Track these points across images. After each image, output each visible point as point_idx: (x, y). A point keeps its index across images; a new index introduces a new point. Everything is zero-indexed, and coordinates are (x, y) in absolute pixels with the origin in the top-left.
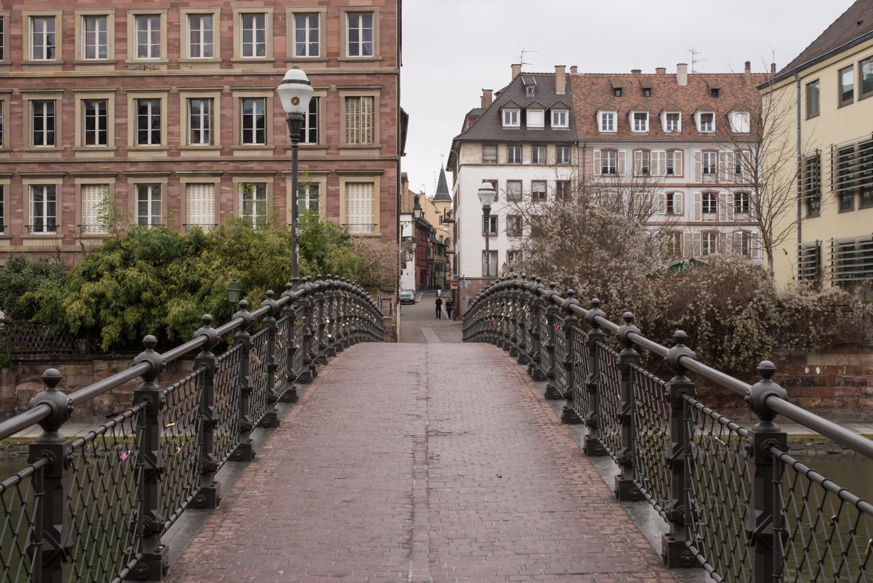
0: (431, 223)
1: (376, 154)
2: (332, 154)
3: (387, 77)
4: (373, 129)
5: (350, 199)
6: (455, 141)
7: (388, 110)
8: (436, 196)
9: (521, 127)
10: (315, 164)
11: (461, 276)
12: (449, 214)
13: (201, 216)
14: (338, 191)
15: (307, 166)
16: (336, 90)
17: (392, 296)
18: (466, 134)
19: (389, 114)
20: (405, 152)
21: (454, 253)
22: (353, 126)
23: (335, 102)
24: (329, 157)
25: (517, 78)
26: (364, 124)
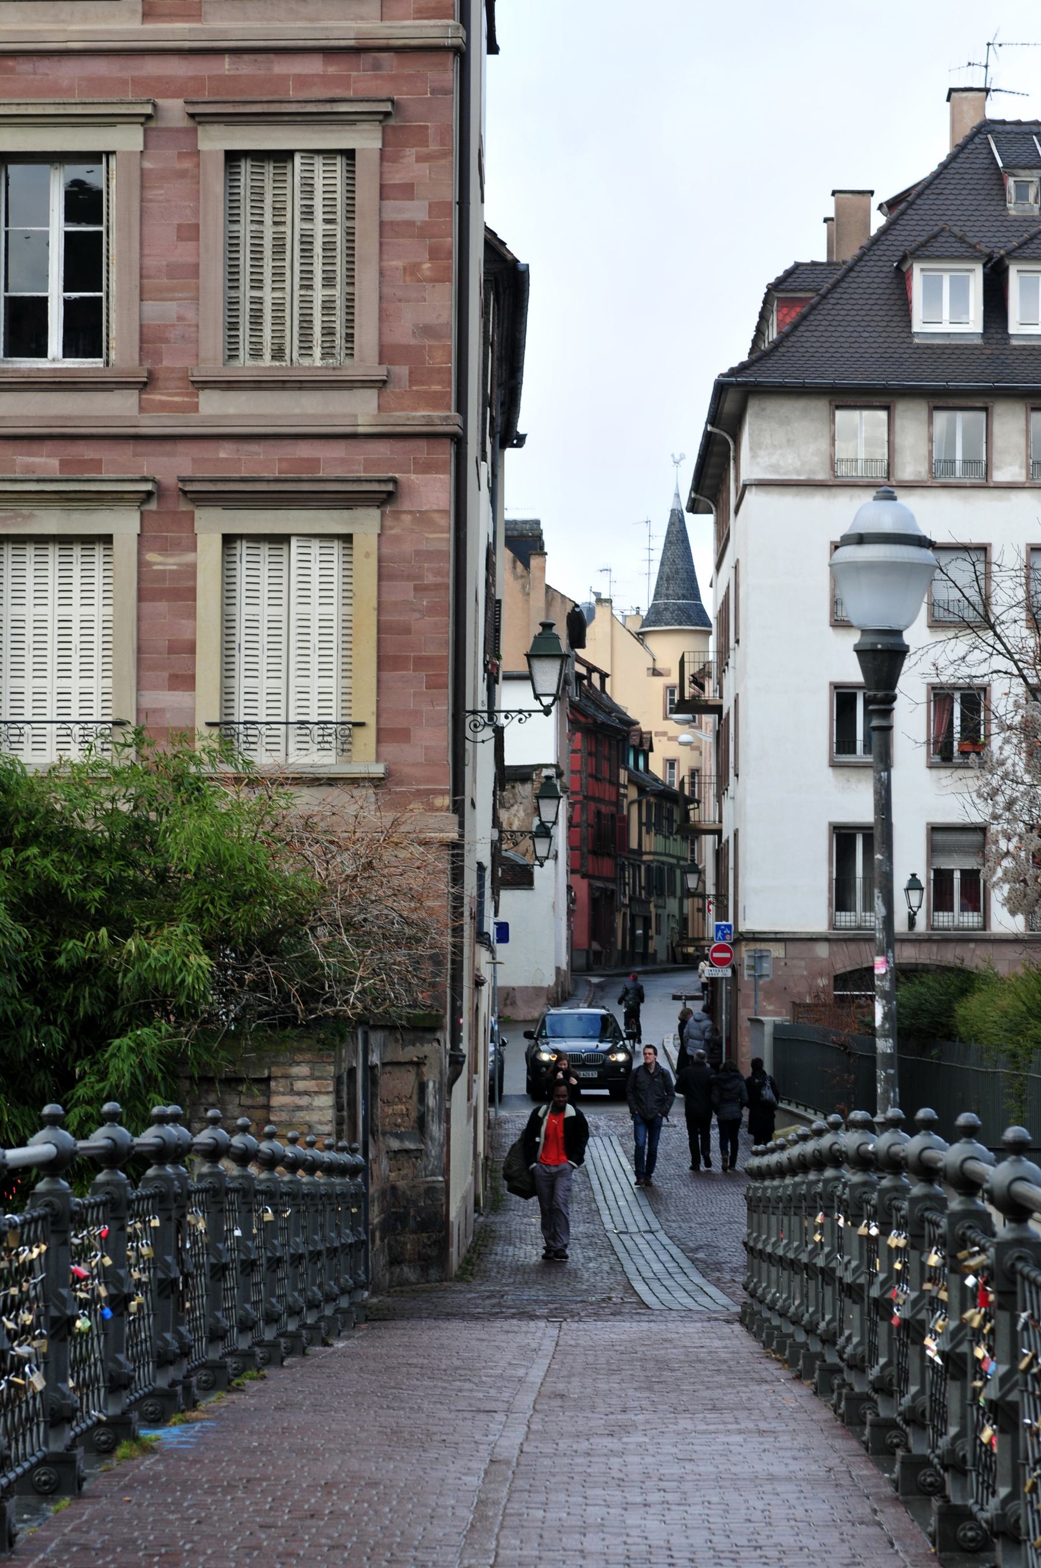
0: (632, 714)
2: (164, 406)
3: (412, 66)
4: (350, 299)
5: (243, 611)
6: (721, 388)
7: (416, 211)
8: (654, 610)
9: (985, 334)
10: (87, 452)
11: (746, 925)
12: (698, 682)
13: (51, 684)
14: (191, 572)
15: (55, 462)
16: (186, 123)
17: (427, 1049)
18: (770, 363)
19: (421, 231)
20: (521, 428)
21: (718, 832)
22: (257, 284)
23: (182, 174)
24: (151, 424)
25: (970, 139)
26: (307, 276)
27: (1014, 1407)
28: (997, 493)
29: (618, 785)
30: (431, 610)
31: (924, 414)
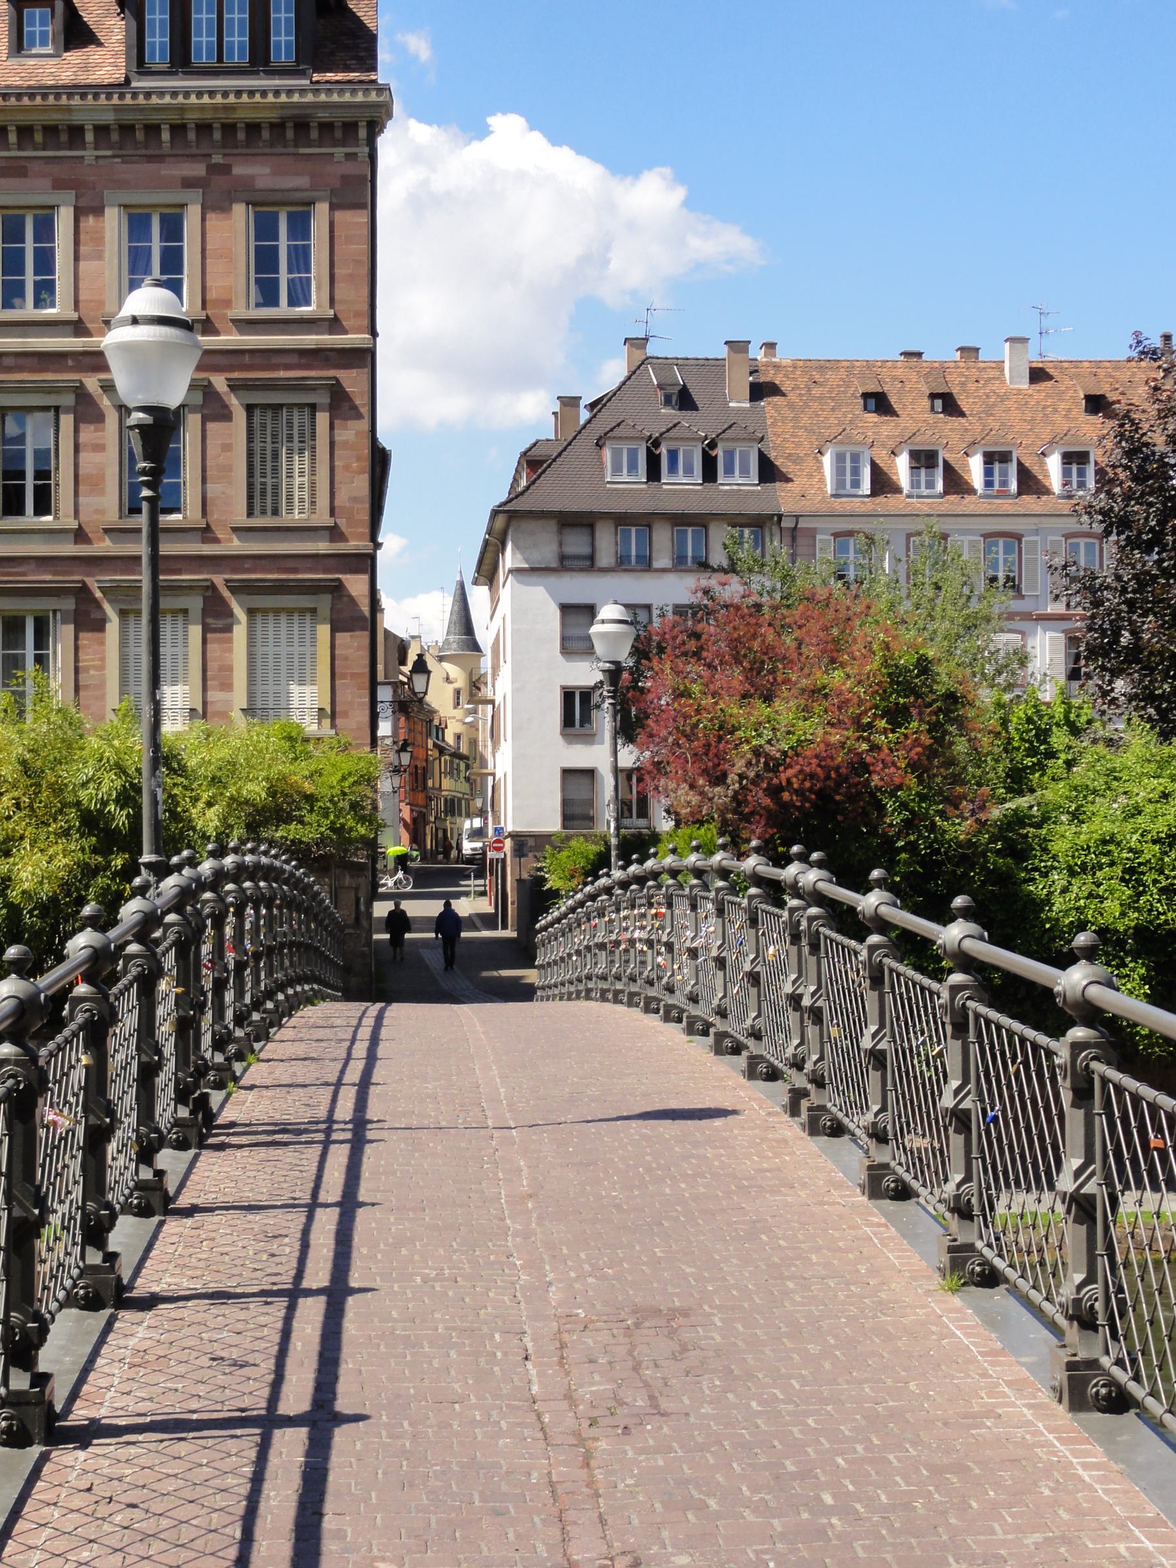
1: (323, 547)
5: (260, 650)
22: (264, 475)
27: (672, 943)
28: (656, 574)
29: (427, 749)
30: (359, 648)
31: (613, 529)
